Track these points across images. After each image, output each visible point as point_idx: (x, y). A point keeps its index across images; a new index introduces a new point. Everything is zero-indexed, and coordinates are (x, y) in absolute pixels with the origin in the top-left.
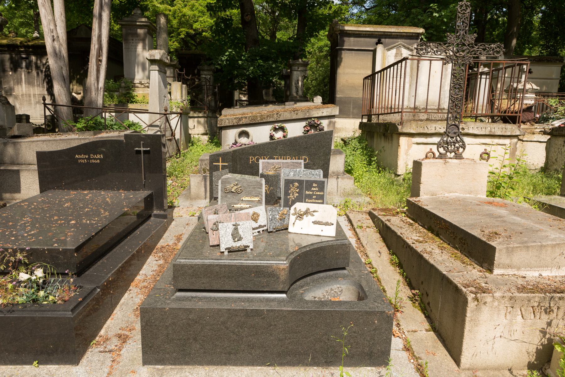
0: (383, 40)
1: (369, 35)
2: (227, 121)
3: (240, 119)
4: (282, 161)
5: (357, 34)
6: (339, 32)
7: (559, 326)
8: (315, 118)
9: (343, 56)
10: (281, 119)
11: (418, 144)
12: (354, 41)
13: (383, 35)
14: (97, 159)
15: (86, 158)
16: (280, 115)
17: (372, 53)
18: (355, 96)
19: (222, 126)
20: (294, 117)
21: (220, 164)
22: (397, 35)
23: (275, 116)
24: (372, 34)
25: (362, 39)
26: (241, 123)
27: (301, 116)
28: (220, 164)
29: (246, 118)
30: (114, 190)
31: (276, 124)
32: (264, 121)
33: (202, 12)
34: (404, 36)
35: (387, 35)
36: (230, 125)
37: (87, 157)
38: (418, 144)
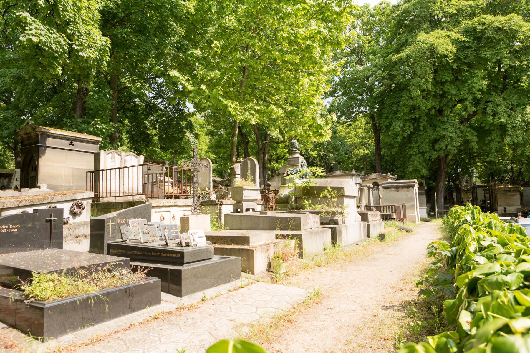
0: (74, 143)
1: (64, 137)
2: (9, 203)
3: (20, 202)
4: (137, 220)
5: (55, 136)
6: (41, 133)
7: (410, 100)
8: (79, 199)
9: (47, 151)
10: (54, 201)
11: (156, 212)
12: (52, 141)
13: (74, 139)
14: (15, 228)
15: (6, 228)
16: (53, 198)
17: (93, 156)
18: (54, 184)
19: (4, 207)
20: (64, 200)
21: (111, 224)
22: (84, 141)
23: (50, 198)
24: (66, 138)
25: (86, 144)
26: (21, 205)
27: (68, 198)
28: (111, 224)
29: (26, 200)
30: (27, 251)
31: (51, 205)
32: (41, 202)
33: (174, 157)
34: (89, 141)
35: (77, 139)
36: (12, 206)
37: (7, 227)
38: (156, 212)
